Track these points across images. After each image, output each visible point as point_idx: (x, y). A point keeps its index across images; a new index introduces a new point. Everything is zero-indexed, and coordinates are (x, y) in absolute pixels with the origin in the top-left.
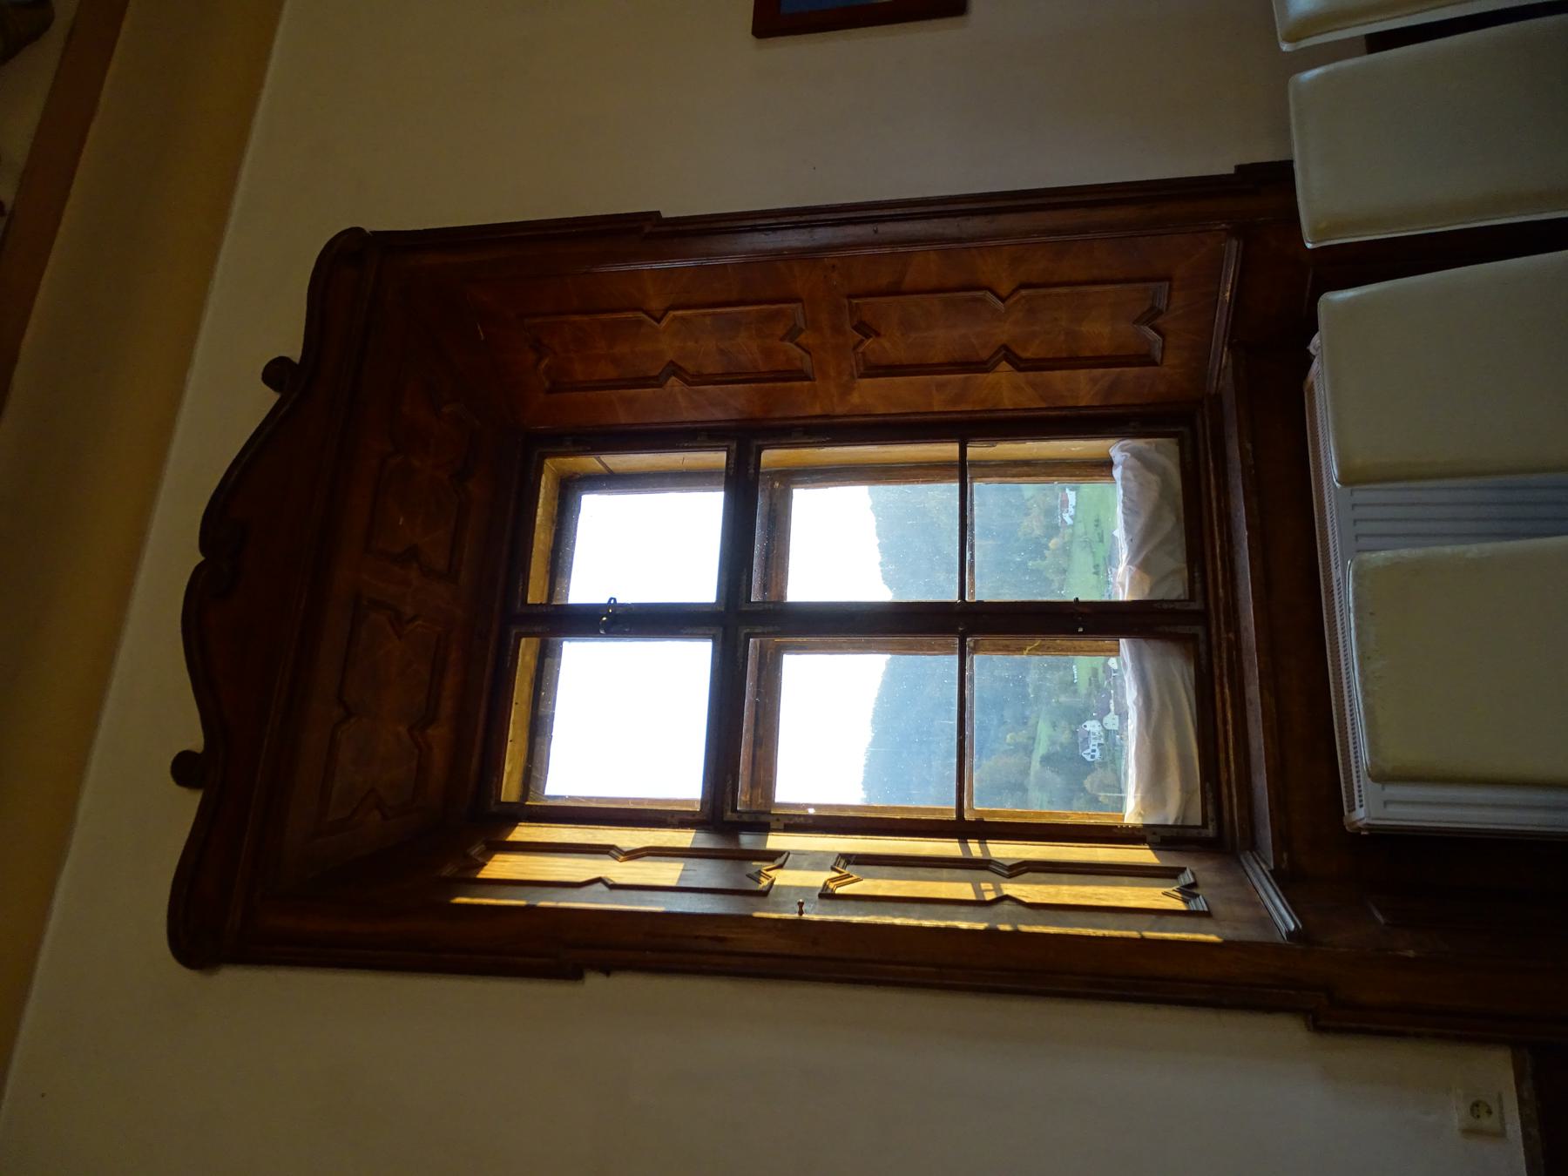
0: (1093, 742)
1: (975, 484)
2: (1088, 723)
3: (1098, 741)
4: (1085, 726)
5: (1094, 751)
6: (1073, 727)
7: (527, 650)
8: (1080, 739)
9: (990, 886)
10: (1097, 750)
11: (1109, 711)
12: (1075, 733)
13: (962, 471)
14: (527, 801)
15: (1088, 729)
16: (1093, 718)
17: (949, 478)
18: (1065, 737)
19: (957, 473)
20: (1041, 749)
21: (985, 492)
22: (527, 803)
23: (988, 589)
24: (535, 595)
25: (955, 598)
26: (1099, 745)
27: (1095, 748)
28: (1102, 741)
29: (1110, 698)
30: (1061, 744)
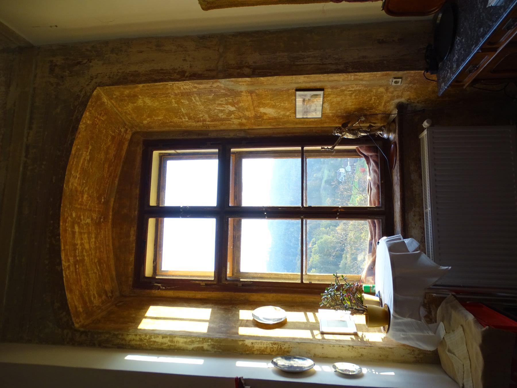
0: (342, 175)
1: (308, 160)
2: (341, 169)
3: (343, 175)
4: (340, 170)
5: (342, 178)
6: (335, 171)
7: (152, 221)
8: (338, 174)
9: (317, 337)
10: (343, 178)
11: (348, 165)
12: (336, 173)
13: (303, 155)
14: (157, 275)
15: (340, 171)
16: (342, 167)
17: (297, 157)
18: (333, 174)
19: (300, 154)
20: (325, 179)
21: (310, 161)
22: (157, 277)
23: (312, 202)
24: (153, 202)
25: (300, 205)
26: (344, 176)
27: (343, 177)
28: (345, 175)
29: (348, 161)
30: (332, 177)
